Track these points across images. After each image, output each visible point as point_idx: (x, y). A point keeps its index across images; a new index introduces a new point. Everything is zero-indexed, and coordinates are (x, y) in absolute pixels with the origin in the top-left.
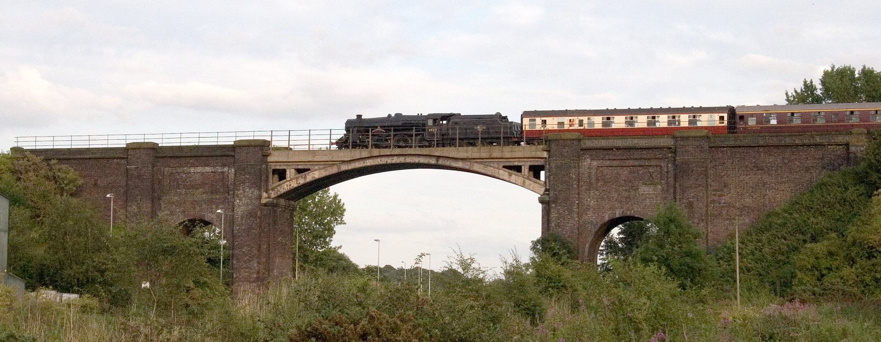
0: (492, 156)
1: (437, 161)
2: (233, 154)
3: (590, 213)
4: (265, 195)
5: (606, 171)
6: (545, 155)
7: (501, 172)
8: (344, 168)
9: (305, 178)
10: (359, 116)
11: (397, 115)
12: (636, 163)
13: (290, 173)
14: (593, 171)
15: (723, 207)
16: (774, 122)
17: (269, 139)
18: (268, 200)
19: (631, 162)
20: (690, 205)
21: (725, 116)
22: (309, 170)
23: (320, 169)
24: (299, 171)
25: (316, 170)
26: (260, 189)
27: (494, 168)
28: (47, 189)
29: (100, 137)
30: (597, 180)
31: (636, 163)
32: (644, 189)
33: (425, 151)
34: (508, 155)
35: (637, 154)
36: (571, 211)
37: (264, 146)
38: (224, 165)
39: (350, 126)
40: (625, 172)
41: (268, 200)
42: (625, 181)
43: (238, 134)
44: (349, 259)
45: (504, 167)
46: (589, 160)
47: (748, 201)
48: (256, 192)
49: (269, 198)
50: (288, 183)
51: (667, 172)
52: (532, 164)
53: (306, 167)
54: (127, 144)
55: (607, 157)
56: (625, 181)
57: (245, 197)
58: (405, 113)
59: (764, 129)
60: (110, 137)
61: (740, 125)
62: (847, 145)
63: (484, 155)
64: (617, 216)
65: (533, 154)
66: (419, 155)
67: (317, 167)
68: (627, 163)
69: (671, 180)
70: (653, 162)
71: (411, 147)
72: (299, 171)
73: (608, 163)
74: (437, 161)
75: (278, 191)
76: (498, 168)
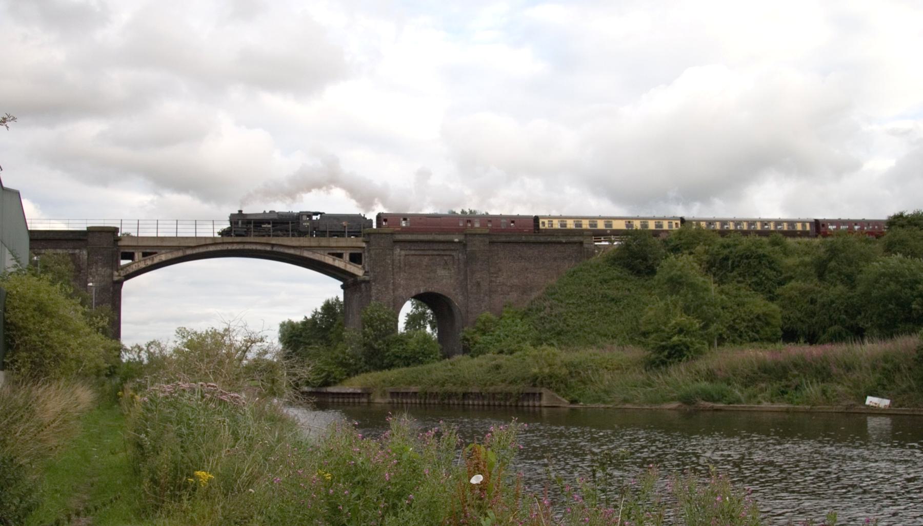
0: (321, 245)
1: (272, 248)
2: (85, 238)
3: (401, 290)
4: (116, 273)
5: (411, 258)
6: (364, 245)
7: (327, 258)
8: (189, 252)
9: (153, 260)
10: (240, 211)
11: (270, 212)
12: (435, 253)
13: (138, 256)
14: (402, 258)
15: (498, 285)
16: (404, 224)
17: (119, 226)
18: (119, 278)
19: (430, 252)
20: (478, 284)
21: (679, 222)
22: (155, 253)
23: (167, 253)
24: (145, 255)
25: (163, 254)
26: (112, 269)
27: (321, 254)
28: (827, 272)
29: (149, 222)
30: (405, 265)
31: (435, 253)
32: (441, 272)
33: (263, 240)
34: (334, 245)
35: (436, 246)
36: (387, 288)
37: (116, 230)
38: (74, 248)
39: (234, 219)
40: (426, 260)
41: (119, 278)
42: (426, 266)
43: (88, 222)
44: (280, 331)
45: (329, 254)
46: (399, 250)
47: (515, 281)
48: (109, 271)
49: (119, 276)
50: (136, 264)
51: (459, 260)
52: (353, 252)
53: (154, 251)
54: (87, 228)
55: (413, 248)
56: (426, 266)
57: (98, 275)
58: (503, 214)
59: (553, 232)
60: (70, 221)
61: (822, 229)
62: (581, 243)
63: (313, 244)
64: (422, 292)
65: (354, 244)
66: (232, 243)
67: (163, 251)
68: (427, 253)
69: (462, 266)
70: (448, 253)
71: (269, 236)
72: (145, 255)
73: (413, 252)
74: (272, 248)
75: (128, 270)
76: (324, 255)
